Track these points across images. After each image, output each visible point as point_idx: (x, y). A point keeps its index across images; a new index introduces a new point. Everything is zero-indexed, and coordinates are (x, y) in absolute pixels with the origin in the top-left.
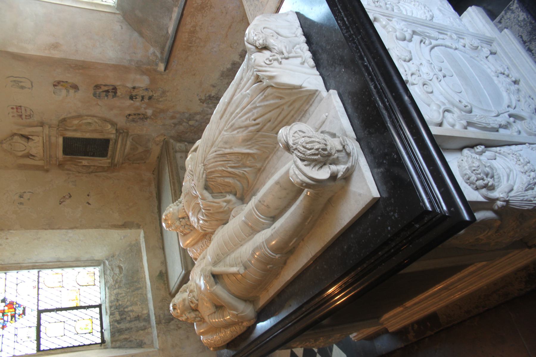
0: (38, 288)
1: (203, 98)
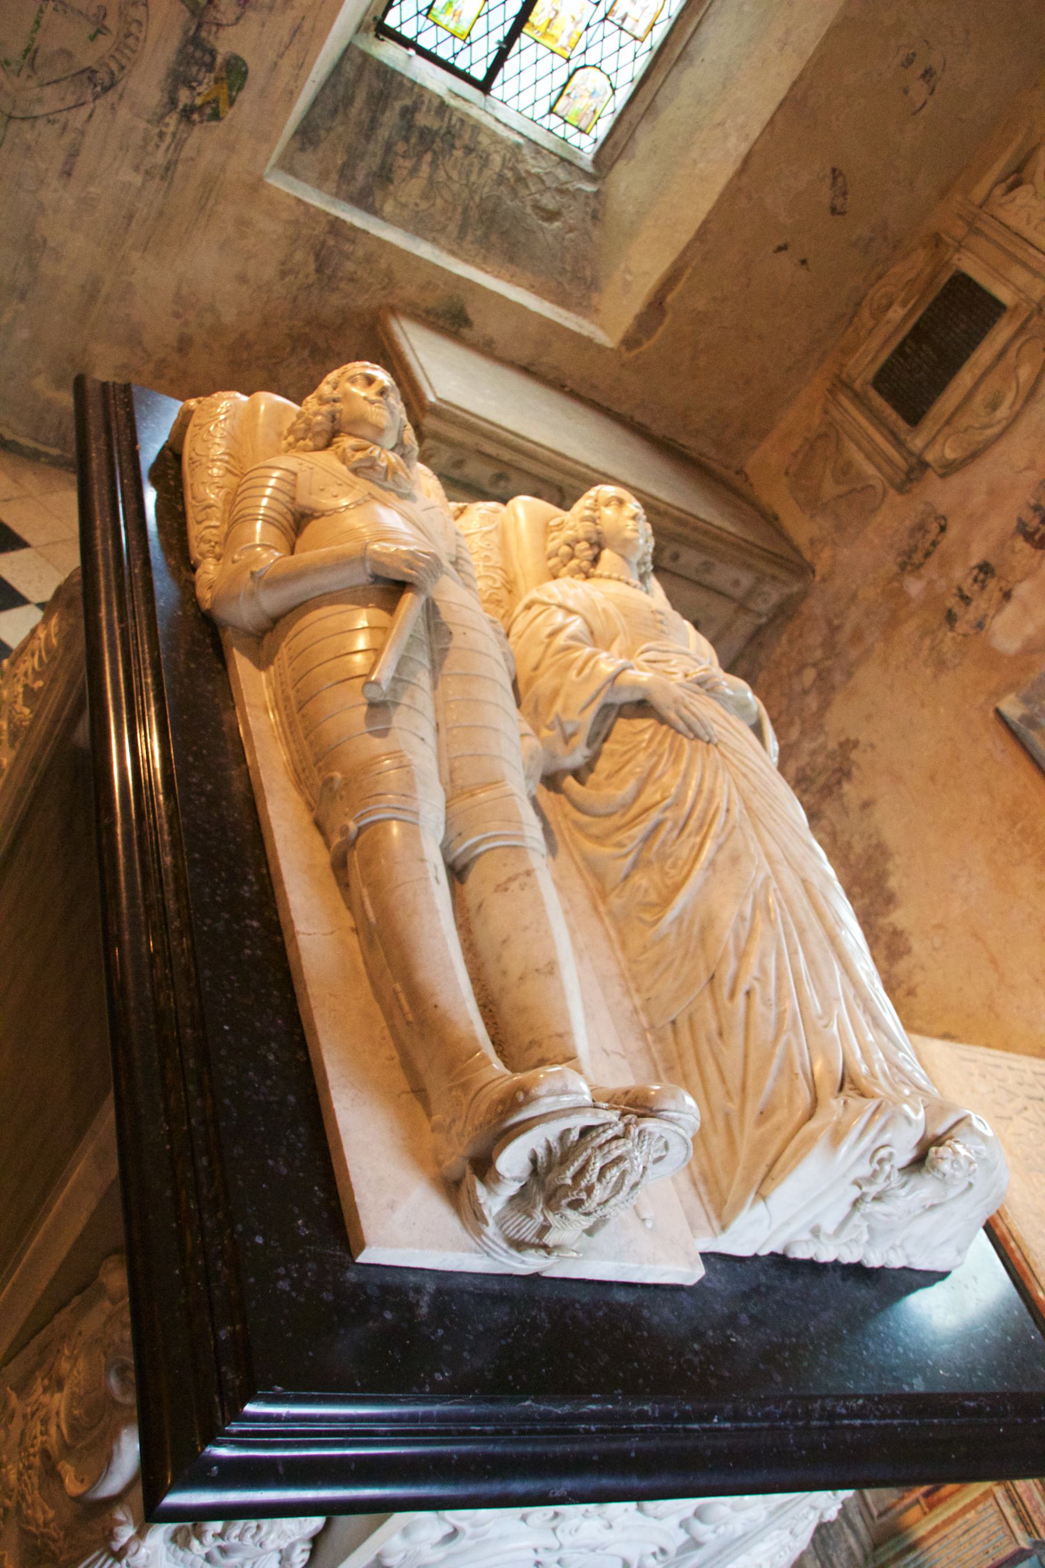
1: (854, 755)
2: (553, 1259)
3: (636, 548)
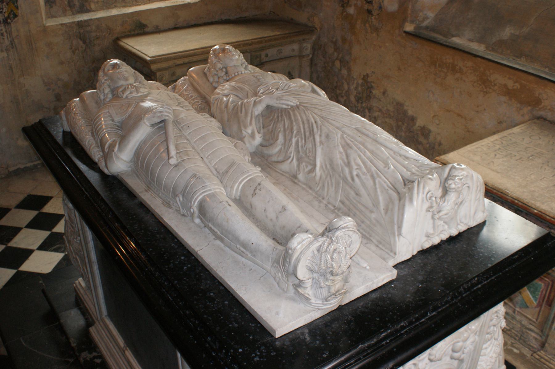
1: (369, 80)
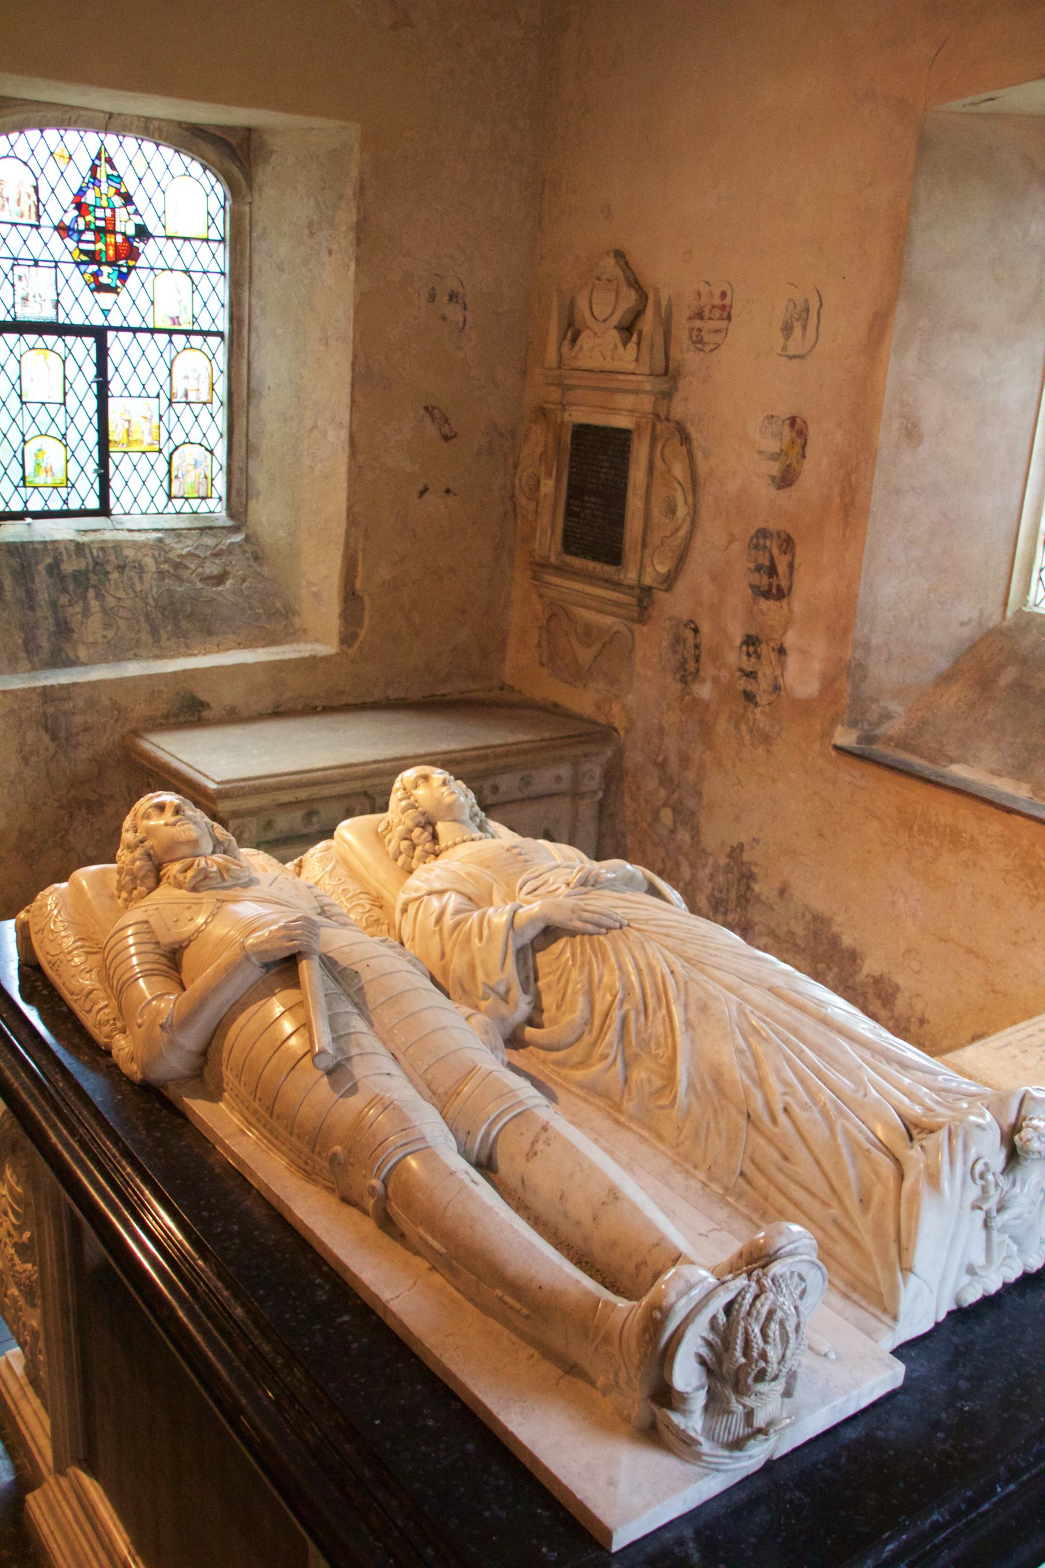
0: (170, 332)
1: (746, 857)
2: (773, 1438)
3: (462, 806)
